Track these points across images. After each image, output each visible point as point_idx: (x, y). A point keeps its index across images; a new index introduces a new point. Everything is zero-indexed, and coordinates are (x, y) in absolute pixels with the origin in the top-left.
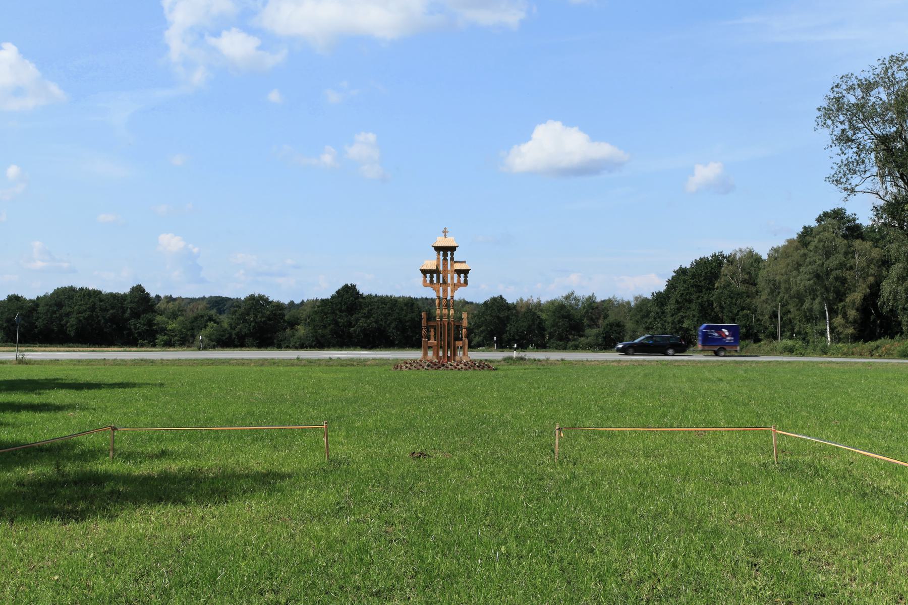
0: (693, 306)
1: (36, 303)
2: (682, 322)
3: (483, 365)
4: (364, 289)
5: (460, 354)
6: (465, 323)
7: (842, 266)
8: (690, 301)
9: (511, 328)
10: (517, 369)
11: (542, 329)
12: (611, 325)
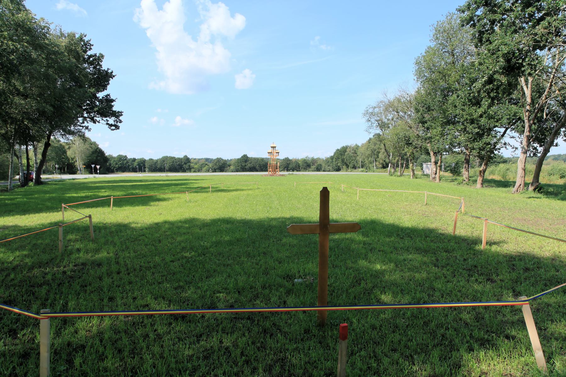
0: (340, 159)
1: (157, 161)
2: (337, 164)
3: (282, 175)
4: (249, 156)
5: (277, 173)
6: (278, 165)
7: (379, 148)
8: (339, 158)
9: (290, 166)
10: (291, 176)
11: (299, 166)
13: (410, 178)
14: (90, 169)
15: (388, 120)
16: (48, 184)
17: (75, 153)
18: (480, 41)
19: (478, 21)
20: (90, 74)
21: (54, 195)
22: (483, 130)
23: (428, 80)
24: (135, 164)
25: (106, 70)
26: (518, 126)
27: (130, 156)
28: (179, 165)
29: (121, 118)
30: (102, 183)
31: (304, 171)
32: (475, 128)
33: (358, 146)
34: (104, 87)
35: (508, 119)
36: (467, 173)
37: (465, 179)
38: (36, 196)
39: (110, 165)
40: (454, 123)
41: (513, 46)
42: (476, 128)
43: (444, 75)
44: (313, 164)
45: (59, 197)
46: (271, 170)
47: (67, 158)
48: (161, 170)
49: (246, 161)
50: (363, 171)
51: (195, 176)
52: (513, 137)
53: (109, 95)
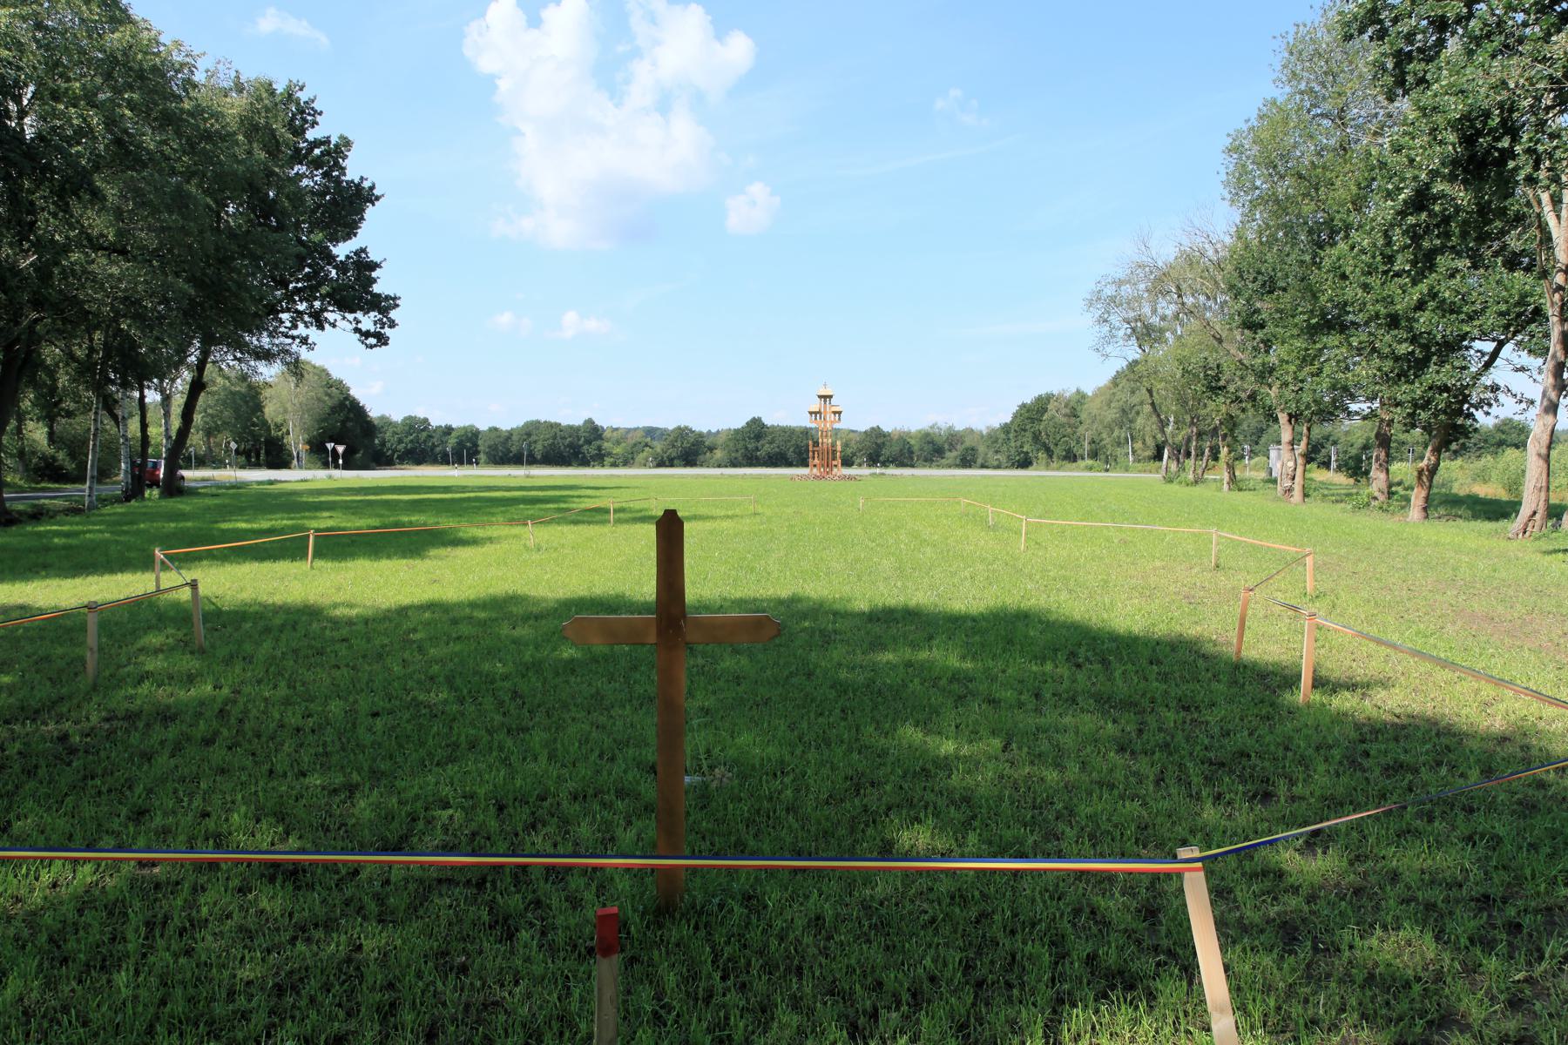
0: (1027, 434)
1: (510, 434)
2: (1022, 447)
3: (850, 478)
4: (768, 421)
5: (835, 470)
6: (839, 448)
8: (1025, 430)
9: (886, 452)
12: (967, 449)
13: (1220, 489)
14: (320, 454)
15: (1163, 318)
16: (199, 494)
17: (286, 411)
18: (1400, 82)
19: (1395, 21)
20: (312, 193)
21: (189, 524)
22: (1426, 347)
23: (1279, 205)
24: (452, 441)
25: (357, 181)
26: (1533, 336)
27: (437, 420)
28: (571, 445)
29: (393, 314)
30: (340, 495)
31: (924, 466)
32: (1400, 342)
33: (1084, 396)
34: (350, 230)
35: (1501, 314)
36: (1382, 476)
37: (1376, 494)
38: (142, 526)
39: (383, 443)
40: (1343, 328)
41: (1484, 96)
42: (1406, 340)
43: (1312, 183)
44: (952, 447)
45: (201, 529)
46: (816, 461)
47: (265, 424)
48: (516, 460)
49: (758, 437)
50: (1090, 469)
51: (607, 477)
52: (1522, 369)
53: (363, 250)
